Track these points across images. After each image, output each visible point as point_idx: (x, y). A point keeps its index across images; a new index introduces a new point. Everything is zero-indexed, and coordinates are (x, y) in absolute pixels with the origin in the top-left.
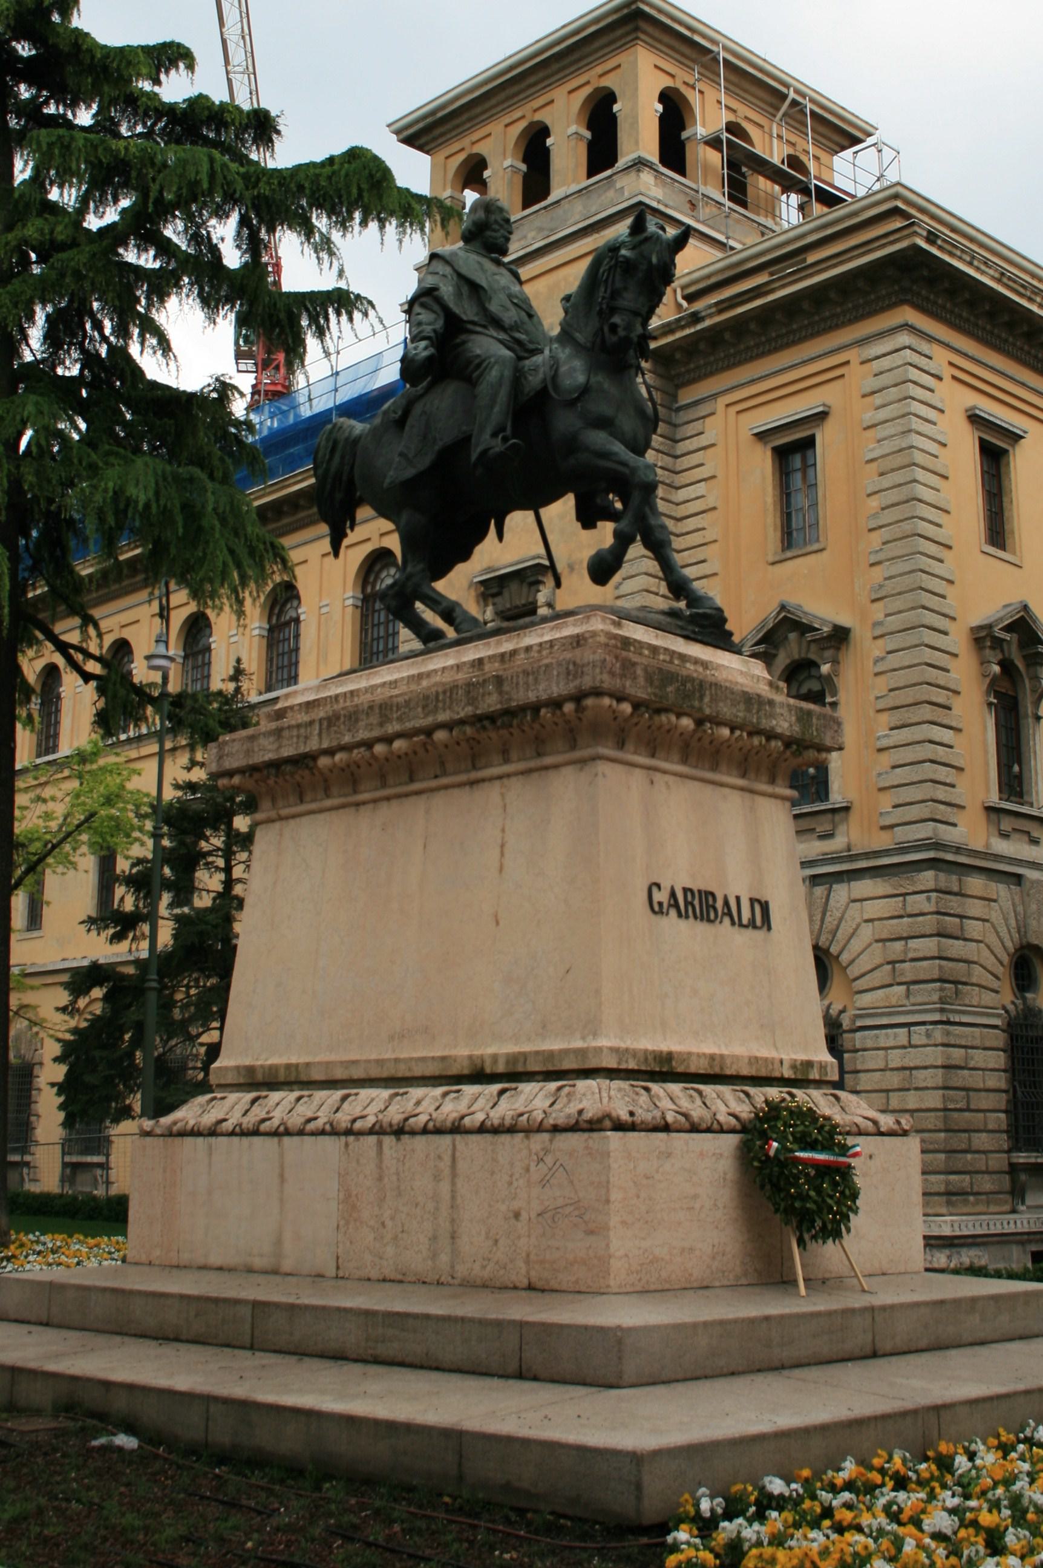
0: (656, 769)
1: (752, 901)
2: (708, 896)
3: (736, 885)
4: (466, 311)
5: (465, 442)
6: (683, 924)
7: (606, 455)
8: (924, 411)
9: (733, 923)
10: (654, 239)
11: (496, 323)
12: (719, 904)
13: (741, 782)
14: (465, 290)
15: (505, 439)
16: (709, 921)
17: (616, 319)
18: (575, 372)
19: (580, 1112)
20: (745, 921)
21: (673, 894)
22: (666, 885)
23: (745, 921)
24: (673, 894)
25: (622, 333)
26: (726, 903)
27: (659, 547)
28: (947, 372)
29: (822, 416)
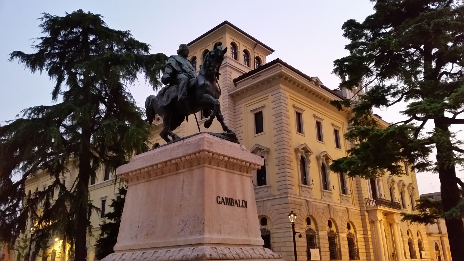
0: (219, 169)
1: (242, 201)
2: (231, 200)
3: (239, 197)
4: (178, 69)
5: (176, 97)
6: (225, 206)
7: (208, 99)
8: (284, 105)
9: (238, 206)
10: (219, 50)
11: (184, 71)
12: (234, 202)
13: (239, 173)
14: (178, 64)
15: (185, 96)
16: (232, 205)
17: (211, 68)
18: (202, 81)
19: (198, 255)
20: (241, 205)
21: (223, 199)
22: (221, 197)
23: (241, 205)
24: (223, 199)
25: (212, 71)
26: (236, 201)
27: (221, 119)
28: (289, 97)
29: (264, 107)
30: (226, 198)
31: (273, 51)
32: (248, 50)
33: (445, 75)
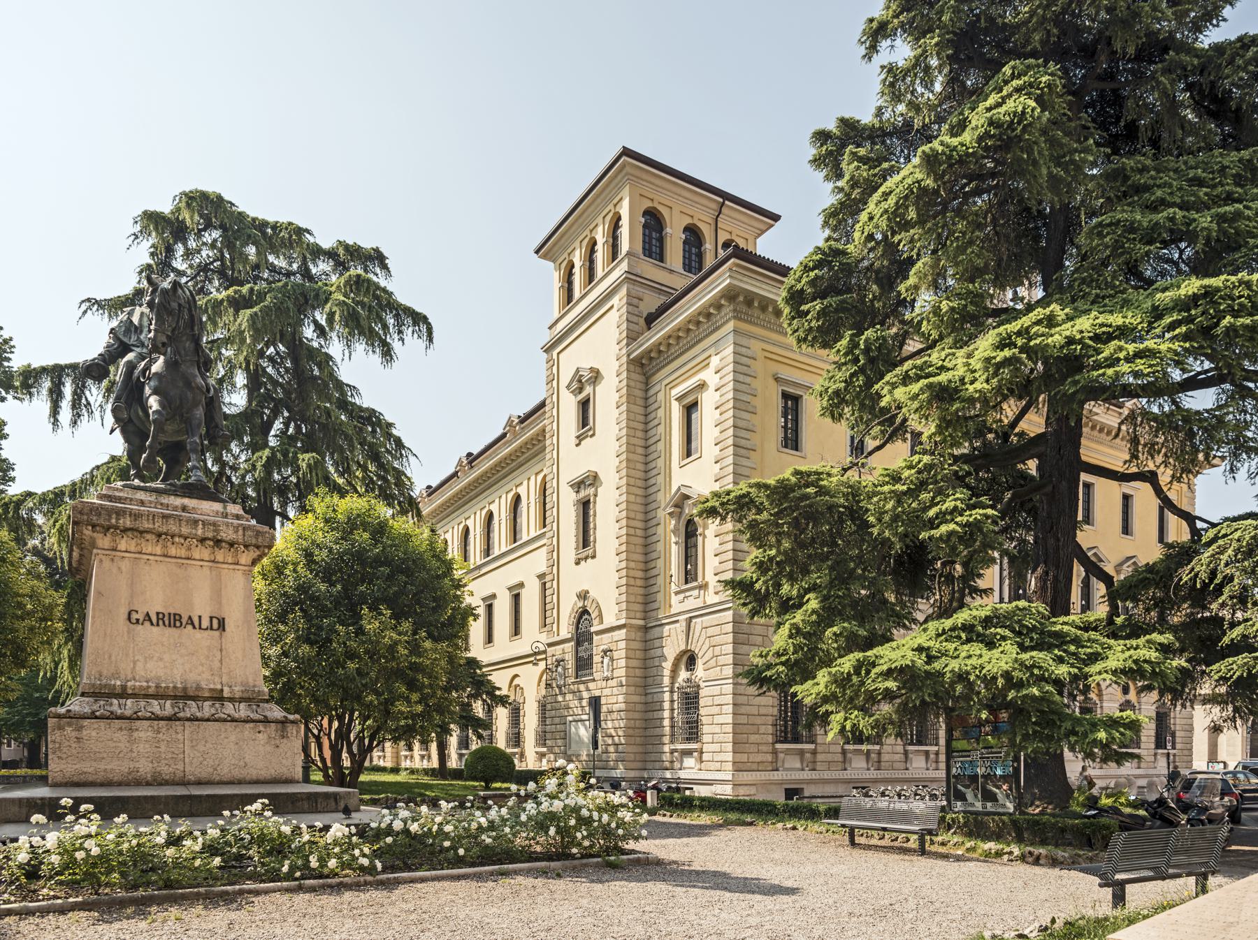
3: (202, 608)
6: (155, 629)
30: (158, 614)
31: (776, 218)
32: (700, 225)
33: (332, 263)
